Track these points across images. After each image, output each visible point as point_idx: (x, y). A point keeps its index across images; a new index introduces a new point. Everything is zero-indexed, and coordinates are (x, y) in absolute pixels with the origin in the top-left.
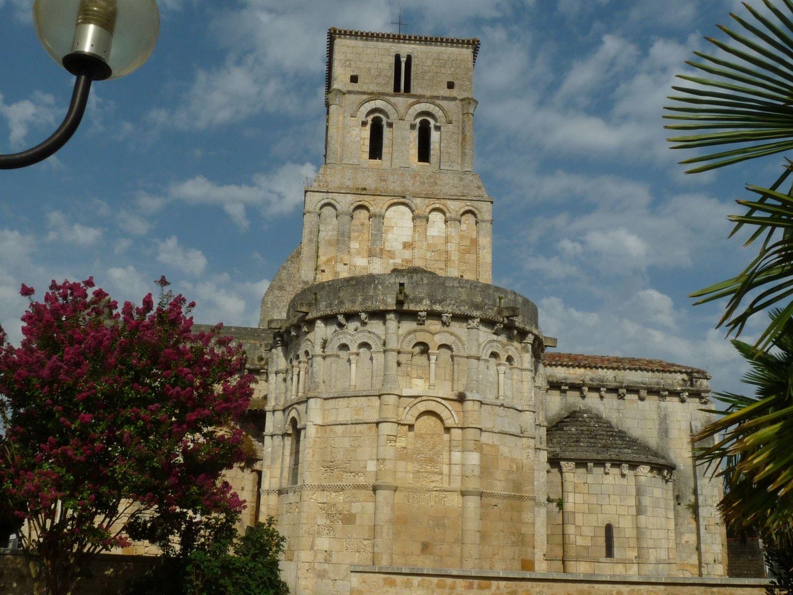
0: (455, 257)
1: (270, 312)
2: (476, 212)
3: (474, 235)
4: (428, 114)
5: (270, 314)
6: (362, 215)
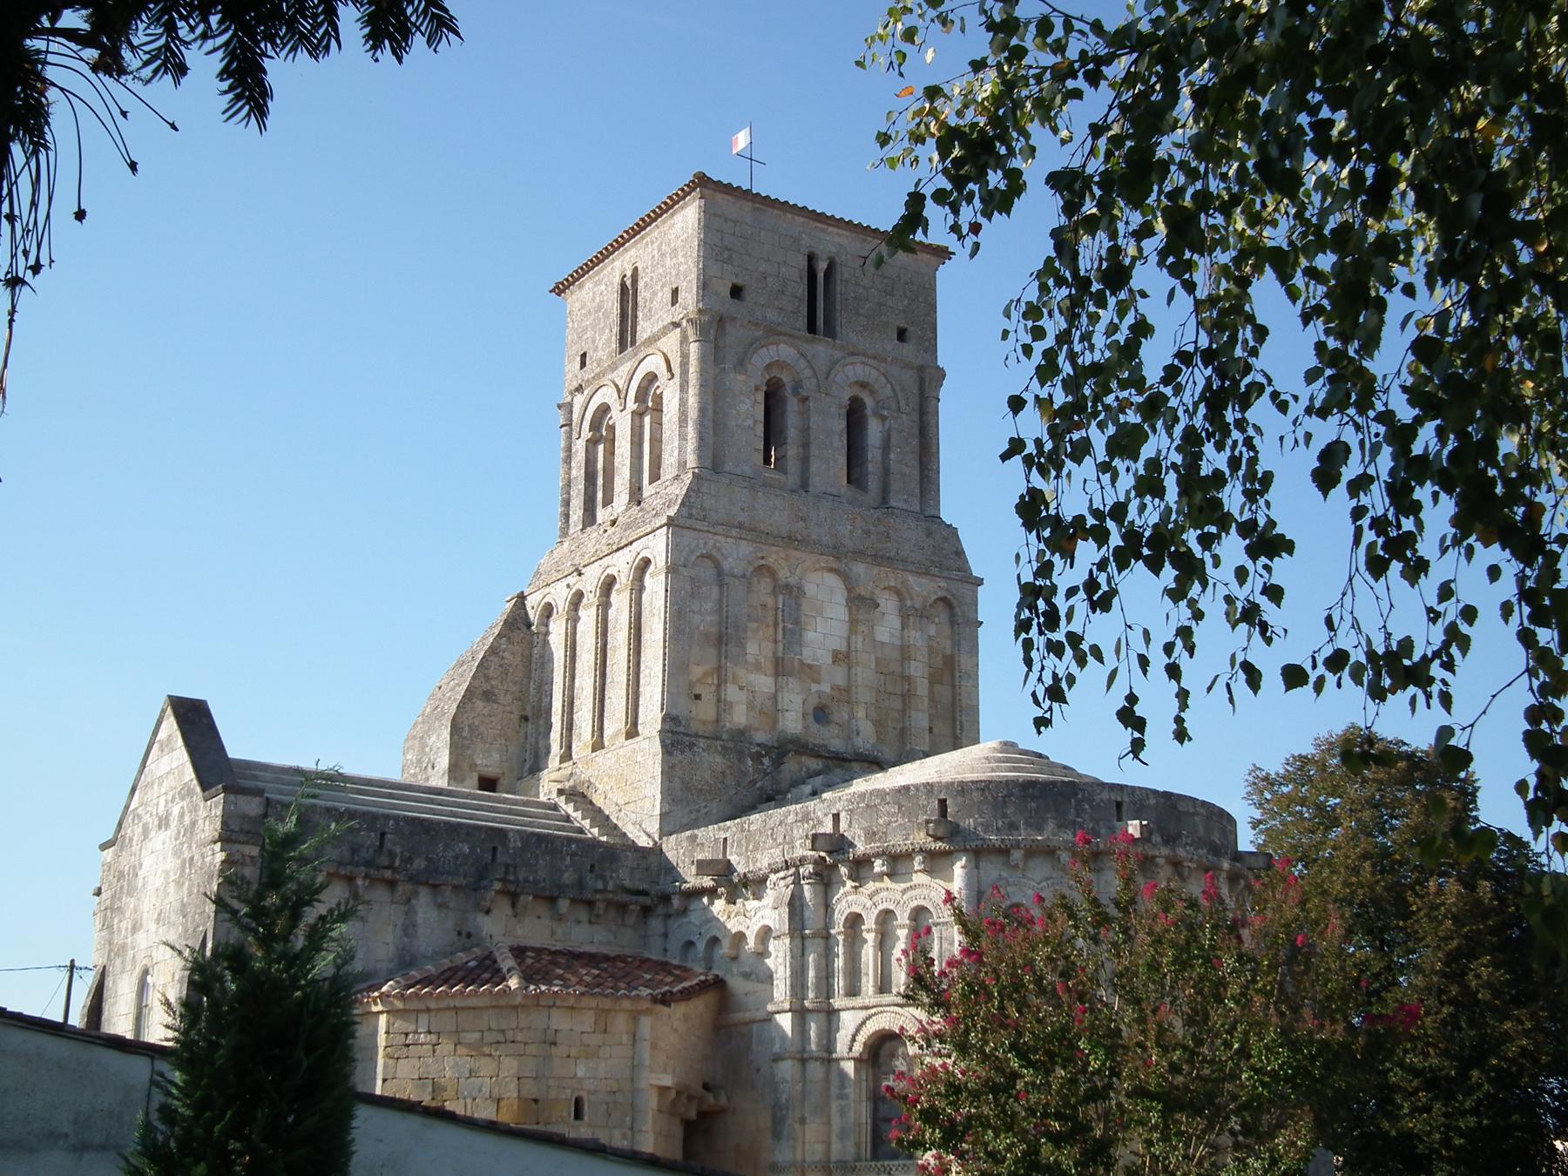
0: (922, 689)
1: (468, 748)
2: (955, 603)
3: (947, 646)
4: (863, 385)
5: (469, 752)
6: (764, 586)
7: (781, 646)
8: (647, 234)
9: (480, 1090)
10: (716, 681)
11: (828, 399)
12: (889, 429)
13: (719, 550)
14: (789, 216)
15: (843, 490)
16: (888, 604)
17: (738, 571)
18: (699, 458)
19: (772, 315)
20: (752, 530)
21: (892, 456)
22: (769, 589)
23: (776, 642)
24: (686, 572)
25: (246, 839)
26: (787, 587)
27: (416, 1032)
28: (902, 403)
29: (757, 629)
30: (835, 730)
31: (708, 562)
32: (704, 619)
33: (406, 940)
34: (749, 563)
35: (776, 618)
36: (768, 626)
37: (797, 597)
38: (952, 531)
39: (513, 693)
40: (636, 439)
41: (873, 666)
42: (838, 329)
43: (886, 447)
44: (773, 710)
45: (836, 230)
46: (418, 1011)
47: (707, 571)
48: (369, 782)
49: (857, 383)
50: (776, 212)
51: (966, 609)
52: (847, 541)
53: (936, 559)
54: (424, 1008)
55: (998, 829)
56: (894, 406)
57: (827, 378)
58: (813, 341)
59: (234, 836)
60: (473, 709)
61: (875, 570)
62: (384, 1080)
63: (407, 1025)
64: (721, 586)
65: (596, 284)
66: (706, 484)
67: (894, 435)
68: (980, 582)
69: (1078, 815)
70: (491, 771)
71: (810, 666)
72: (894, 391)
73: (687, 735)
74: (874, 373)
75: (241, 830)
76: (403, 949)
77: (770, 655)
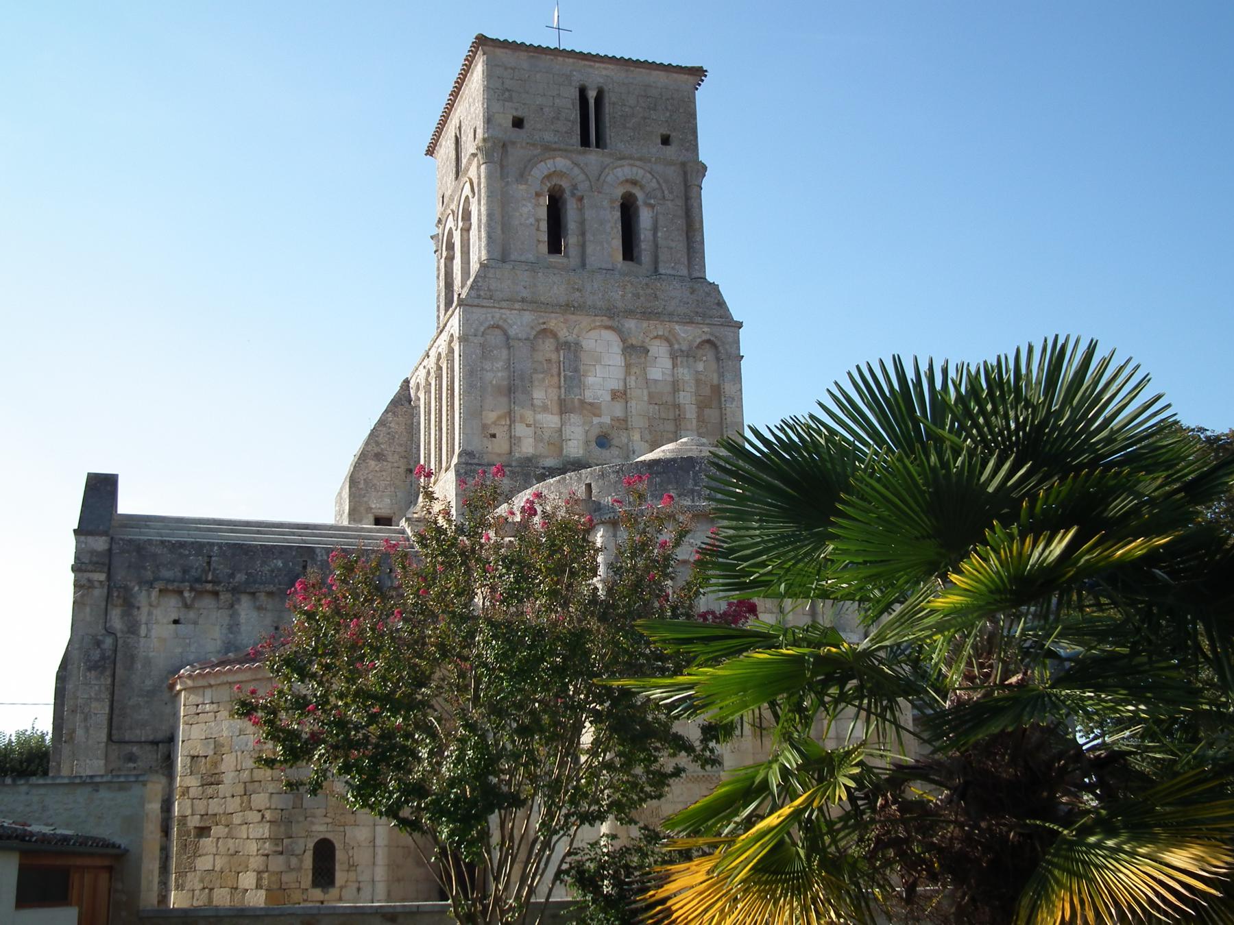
2: (719, 344)
4: (634, 183)
5: (365, 499)
6: (548, 346)
7: (563, 390)
8: (463, 93)
9: (247, 745)
10: (508, 423)
11: (600, 196)
12: (657, 215)
13: (505, 321)
14: (560, 59)
15: (619, 266)
16: (659, 351)
17: (523, 335)
18: (488, 252)
19: (548, 137)
20: (532, 302)
21: (659, 234)
22: (553, 348)
23: (560, 387)
24: (476, 340)
25: (93, 568)
26: (567, 345)
27: (203, 704)
28: (666, 192)
29: (544, 379)
30: (615, 452)
31: (497, 332)
32: (496, 373)
33: (231, 636)
34: (532, 328)
35: (560, 369)
36: (552, 376)
37: (576, 351)
38: (715, 287)
39: (399, 453)
40: (465, 249)
41: (646, 398)
42: (608, 141)
43: (655, 229)
44: (559, 441)
45: (602, 65)
46: (204, 687)
47: (496, 338)
48: (315, 527)
49: (627, 181)
50: (548, 57)
51: (727, 347)
52: (619, 304)
53: (700, 310)
54: (206, 684)
55: (630, 502)
56: (659, 195)
57: (598, 180)
58: (584, 153)
59: (84, 567)
60: (367, 467)
61: (645, 324)
62: (183, 741)
63: (197, 698)
64: (509, 348)
65: (446, 141)
66: (492, 271)
67: (661, 217)
68: (739, 325)
69: (696, 485)
70: (384, 512)
71: (591, 404)
72: (658, 182)
73: (480, 465)
74: (641, 172)
75: (91, 562)
76: (228, 643)
77: (556, 398)
